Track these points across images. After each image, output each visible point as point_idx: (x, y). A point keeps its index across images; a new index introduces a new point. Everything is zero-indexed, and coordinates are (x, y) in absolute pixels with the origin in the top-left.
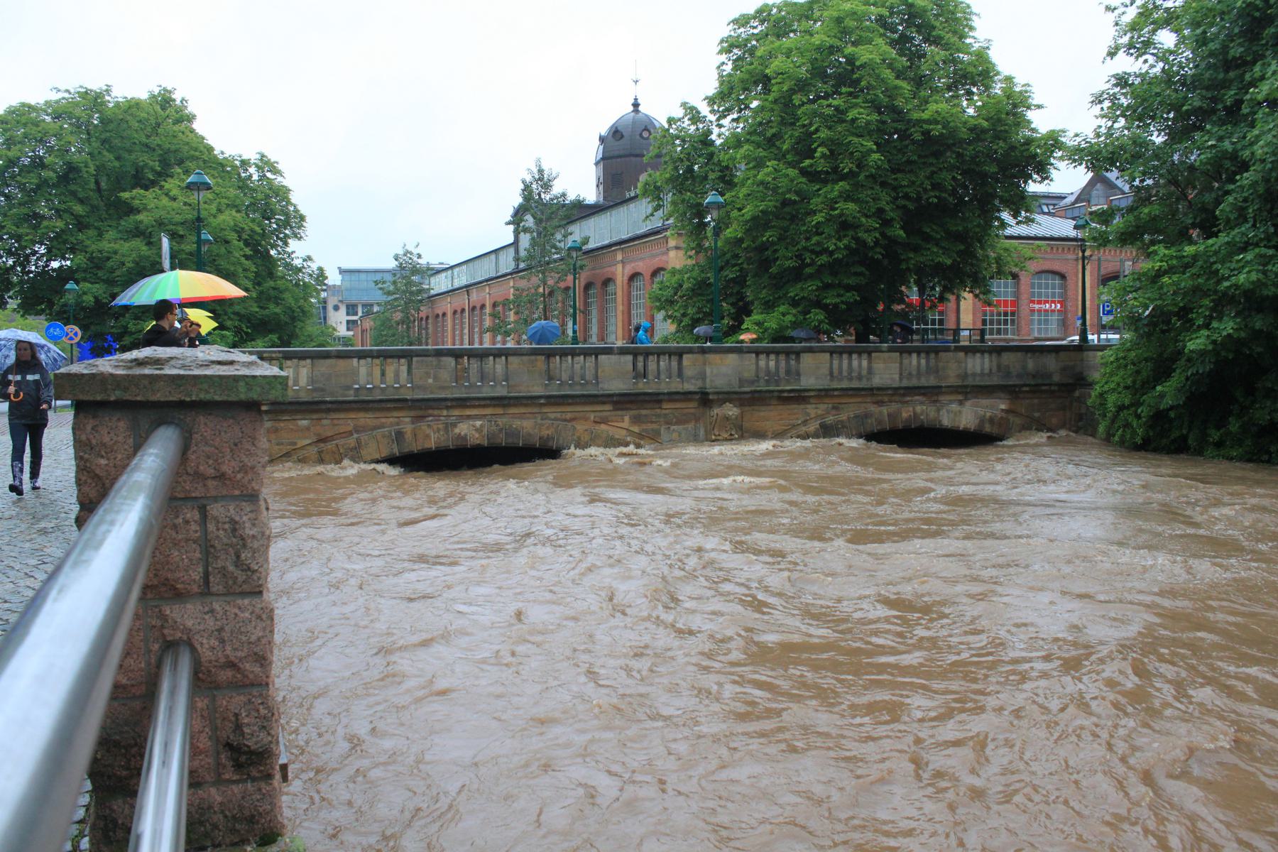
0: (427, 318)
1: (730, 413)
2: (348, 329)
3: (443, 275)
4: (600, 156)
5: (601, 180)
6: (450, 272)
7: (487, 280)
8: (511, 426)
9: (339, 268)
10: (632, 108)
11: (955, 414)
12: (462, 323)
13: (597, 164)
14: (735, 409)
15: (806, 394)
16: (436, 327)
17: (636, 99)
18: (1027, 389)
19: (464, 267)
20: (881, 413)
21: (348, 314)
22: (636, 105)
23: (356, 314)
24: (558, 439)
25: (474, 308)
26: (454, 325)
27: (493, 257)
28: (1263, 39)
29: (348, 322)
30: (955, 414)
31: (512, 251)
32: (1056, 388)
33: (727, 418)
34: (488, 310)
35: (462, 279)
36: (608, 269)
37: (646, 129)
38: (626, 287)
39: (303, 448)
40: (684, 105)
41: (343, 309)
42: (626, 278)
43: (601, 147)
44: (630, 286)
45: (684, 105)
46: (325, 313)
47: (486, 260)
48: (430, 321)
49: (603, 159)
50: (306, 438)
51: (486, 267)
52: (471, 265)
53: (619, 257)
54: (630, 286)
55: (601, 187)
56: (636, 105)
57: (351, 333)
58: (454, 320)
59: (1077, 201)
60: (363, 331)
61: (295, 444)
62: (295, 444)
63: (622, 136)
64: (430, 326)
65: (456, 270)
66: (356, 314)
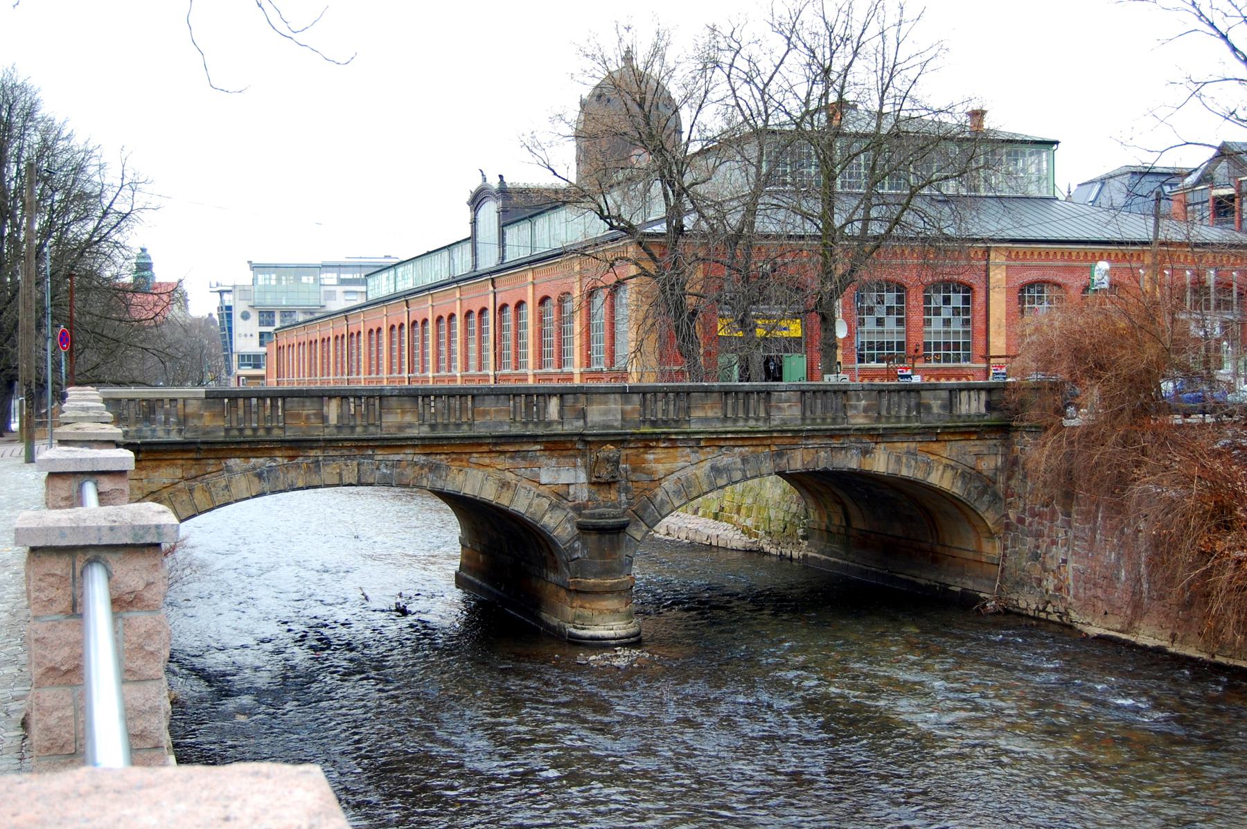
0: (343, 336)
2: (261, 344)
3: (384, 275)
6: (392, 272)
7: (530, 263)
9: (250, 262)
12: (451, 335)
19: (410, 266)
21: (261, 324)
23: (271, 324)
25: (415, 323)
26: (438, 336)
27: (445, 253)
28: (6, 262)
29: (262, 335)
31: (468, 246)
35: (407, 280)
40: (941, 47)
41: (255, 317)
45: (941, 47)
46: (230, 322)
47: (436, 257)
48: (362, 337)
51: (437, 267)
52: (418, 263)
57: (264, 350)
59: (1199, 182)
60: (279, 348)
64: (362, 344)
65: (400, 270)
66: (271, 324)
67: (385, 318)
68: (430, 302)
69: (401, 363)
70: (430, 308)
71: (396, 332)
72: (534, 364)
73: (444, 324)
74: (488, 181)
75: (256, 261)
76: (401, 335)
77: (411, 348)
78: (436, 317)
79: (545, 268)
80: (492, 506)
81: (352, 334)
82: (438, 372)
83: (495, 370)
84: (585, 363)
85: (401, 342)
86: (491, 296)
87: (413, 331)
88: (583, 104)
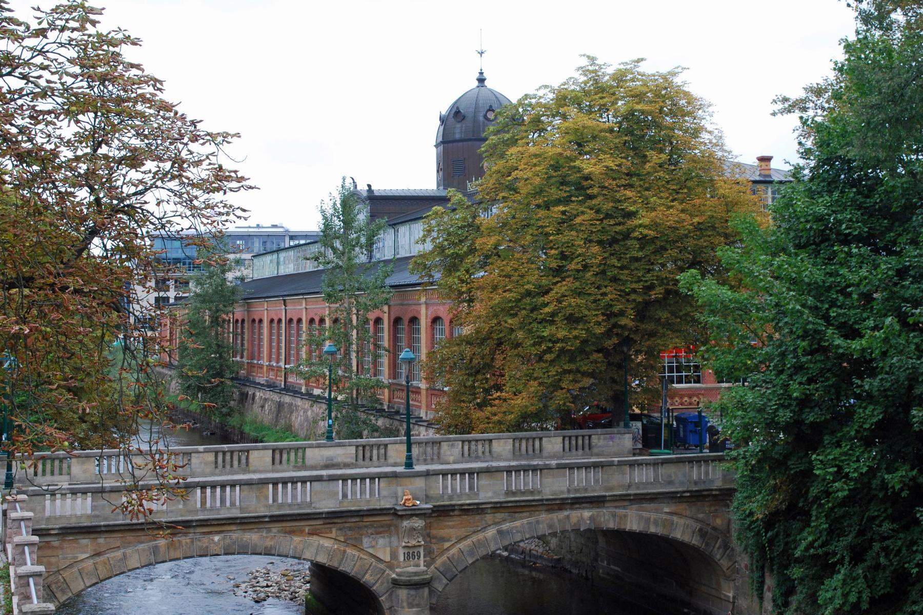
0: (243, 321)
1: (416, 525)
4: (440, 139)
5: (441, 167)
8: (242, 539)
10: (476, 83)
11: (621, 518)
13: (437, 146)
14: (420, 521)
15: (484, 506)
16: (253, 328)
17: (481, 73)
18: (688, 494)
20: (552, 519)
22: (481, 80)
24: (279, 549)
30: (621, 518)
32: (717, 493)
33: (414, 529)
34: (304, 325)
36: (413, 307)
37: (491, 109)
38: (429, 329)
39: (82, 560)
42: (429, 320)
43: (442, 128)
44: (433, 329)
48: (246, 325)
49: (443, 142)
50: (85, 553)
53: (423, 300)
54: (433, 329)
55: (441, 173)
56: (481, 80)
58: (271, 328)
61: (77, 557)
62: (77, 557)
63: (464, 118)
64: (246, 331)
67: (266, 312)
68: (304, 305)
69: (279, 354)
70: (304, 310)
71: (275, 325)
72: (389, 374)
73: (294, 325)
74: (359, 188)
75: (644, 62)
76: (279, 328)
77: (288, 342)
78: (309, 318)
79: (314, 299)
80: (659, 537)
81: (237, 321)
82: (394, 378)
83: (285, 364)
84: (392, 376)
85: (279, 335)
86: (284, 311)
87: (290, 327)
88: (443, 120)
